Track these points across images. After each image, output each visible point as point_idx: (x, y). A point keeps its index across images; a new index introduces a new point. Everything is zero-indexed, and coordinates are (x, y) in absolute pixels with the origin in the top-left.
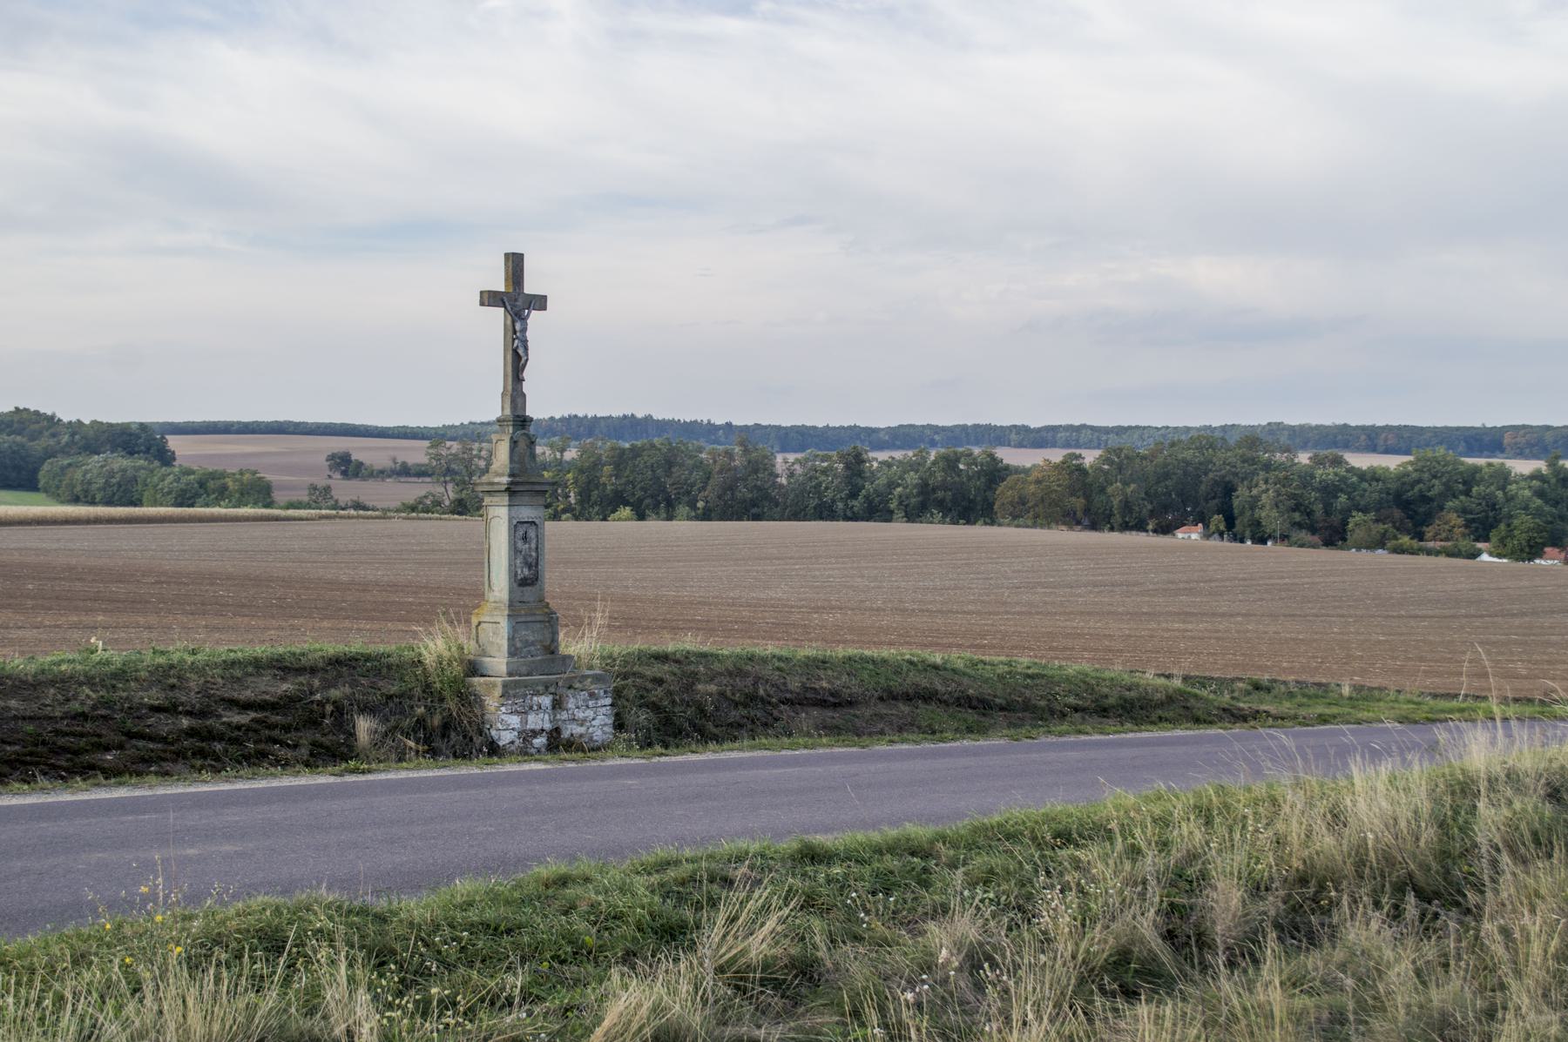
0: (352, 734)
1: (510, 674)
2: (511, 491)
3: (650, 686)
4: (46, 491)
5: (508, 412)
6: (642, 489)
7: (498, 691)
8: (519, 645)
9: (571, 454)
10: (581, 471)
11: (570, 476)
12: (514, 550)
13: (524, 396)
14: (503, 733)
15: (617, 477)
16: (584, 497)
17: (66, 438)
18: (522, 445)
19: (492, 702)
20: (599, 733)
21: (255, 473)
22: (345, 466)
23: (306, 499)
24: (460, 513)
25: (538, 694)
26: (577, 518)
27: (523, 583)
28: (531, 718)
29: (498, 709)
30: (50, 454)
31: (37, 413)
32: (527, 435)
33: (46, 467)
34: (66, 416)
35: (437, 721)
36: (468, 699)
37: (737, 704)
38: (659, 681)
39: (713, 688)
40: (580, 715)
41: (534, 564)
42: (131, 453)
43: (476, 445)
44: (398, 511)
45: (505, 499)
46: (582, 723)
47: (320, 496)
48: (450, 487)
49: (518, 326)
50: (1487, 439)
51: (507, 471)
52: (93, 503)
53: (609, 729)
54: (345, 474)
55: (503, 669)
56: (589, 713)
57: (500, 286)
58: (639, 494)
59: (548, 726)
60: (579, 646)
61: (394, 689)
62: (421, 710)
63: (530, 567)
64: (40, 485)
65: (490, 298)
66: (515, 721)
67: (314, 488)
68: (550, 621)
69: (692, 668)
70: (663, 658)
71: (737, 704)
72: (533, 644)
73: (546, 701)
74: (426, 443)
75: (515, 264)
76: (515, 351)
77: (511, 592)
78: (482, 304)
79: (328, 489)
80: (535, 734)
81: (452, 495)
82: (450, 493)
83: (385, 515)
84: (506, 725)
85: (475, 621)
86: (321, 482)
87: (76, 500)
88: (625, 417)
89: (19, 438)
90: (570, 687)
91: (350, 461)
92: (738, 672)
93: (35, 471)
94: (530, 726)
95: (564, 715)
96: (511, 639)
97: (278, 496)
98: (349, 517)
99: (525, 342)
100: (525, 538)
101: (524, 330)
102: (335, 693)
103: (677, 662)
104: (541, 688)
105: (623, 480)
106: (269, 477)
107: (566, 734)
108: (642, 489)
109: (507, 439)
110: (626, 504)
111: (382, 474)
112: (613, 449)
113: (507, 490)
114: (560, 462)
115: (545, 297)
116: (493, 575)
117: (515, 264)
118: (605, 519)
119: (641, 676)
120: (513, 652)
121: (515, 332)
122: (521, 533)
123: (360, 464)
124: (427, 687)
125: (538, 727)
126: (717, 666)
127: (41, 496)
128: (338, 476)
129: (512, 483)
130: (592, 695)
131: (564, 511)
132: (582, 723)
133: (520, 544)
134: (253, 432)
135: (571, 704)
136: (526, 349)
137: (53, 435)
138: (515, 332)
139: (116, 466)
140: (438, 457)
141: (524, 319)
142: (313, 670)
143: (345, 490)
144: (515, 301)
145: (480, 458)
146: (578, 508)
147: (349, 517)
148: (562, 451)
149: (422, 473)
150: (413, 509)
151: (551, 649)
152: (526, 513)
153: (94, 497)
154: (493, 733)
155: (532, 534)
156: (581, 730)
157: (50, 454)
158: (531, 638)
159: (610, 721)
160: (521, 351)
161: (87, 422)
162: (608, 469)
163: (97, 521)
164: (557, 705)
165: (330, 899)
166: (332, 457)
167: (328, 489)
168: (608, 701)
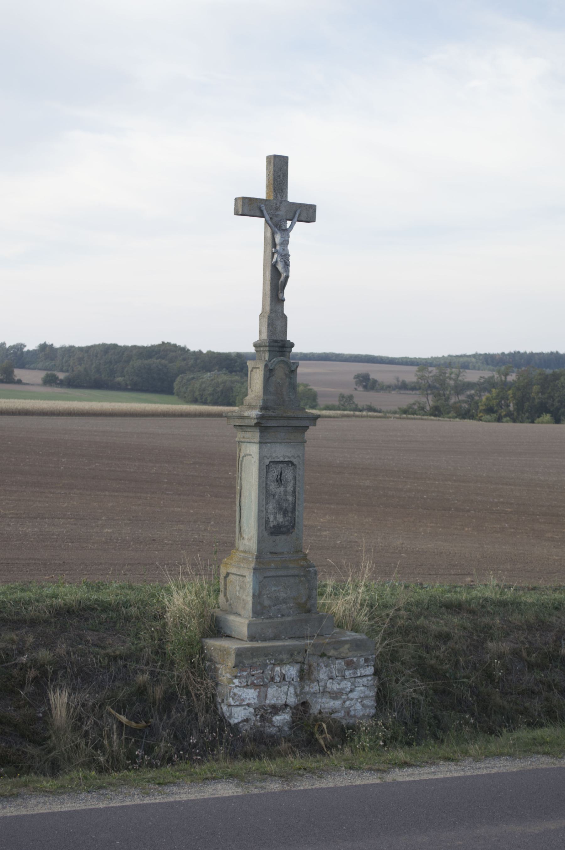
0: (49, 712)
1: (252, 638)
2: (262, 425)
3: (431, 642)
4: (178, 395)
5: (265, 336)
6: (559, 401)
7: (231, 662)
8: (267, 602)
9: (512, 378)
10: (518, 389)
11: (510, 392)
12: (265, 494)
13: (285, 318)
14: (235, 710)
15: (543, 393)
16: (520, 406)
17: (191, 362)
18: (280, 373)
19: (225, 673)
20: (359, 706)
21: (306, 386)
22: (366, 382)
23: (337, 403)
24: (435, 416)
25: (281, 663)
26: (514, 421)
27: (277, 531)
28: (272, 691)
29: (230, 681)
30: (182, 371)
31: (175, 345)
32: (286, 363)
33: (178, 379)
34: (193, 348)
35: (159, 692)
36: (201, 666)
37: (531, 667)
38: (445, 637)
39: (505, 647)
40: (334, 686)
41: (289, 511)
42: (231, 372)
43: (448, 370)
44: (395, 413)
45: (256, 435)
46: (335, 695)
47: (346, 402)
48: (430, 397)
49: (278, 239)
50: (397, 361)
51: (261, 403)
52: (205, 403)
53: (371, 702)
54: (365, 387)
55: (244, 631)
56: (347, 685)
57: (259, 190)
58: (557, 404)
59: (292, 700)
60: (345, 598)
61: (121, 649)
62: (143, 678)
63: (285, 512)
64: (175, 391)
65: (247, 207)
66: (251, 695)
67: (342, 396)
68: (307, 574)
69: (486, 620)
70: (454, 607)
71: (531, 667)
72: (284, 601)
73: (292, 671)
74: (415, 368)
75: (278, 167)
76: (274, 267)
77: (260, 541)
78: (237, 213)
79: (351, 397)
80: (276, 709)
81: (431, 403)
82: (430, 402)
83: (385, 415)
84: (240, 702)
85: (223, 572)
86: (347, 392)
87: (195, 401)
88: (552, 353)
89: (163, 361)
90: (323, 655)
91: (369, 379)
92: (542, 626)
93: (173, 381)
94: (271, 700)
95: (315, 688)
96: (257, 597)
97: (321, 402)
98: (362, 417)
99: (286, 258)
100: (279, 480)
101: (285, 243)
102: (44, 654)
103: (472, 612)
104: (284, 657)
105: (546, 395)
106: (315, 388)
107: (314, 710)
108: (559, 401)
109: (261, 366)
110: (547, 411)
111: (389, 388)
112: (540, 374)
113: (257, 425)
114: (505, 383)
115: (312, 208)
116: (244, 520)
117: (278, 167)
118: (533, 422)
119: (424, 631)
120: (259, 610)
121: (274, 245)
122: (274, 473)
123: (375, 382)
124: (160, 651)
125: (281, 702)
126: (516, 618)
127: (174, 398)
128: (361, 389)
129: (261, 417)
130: (350, 664)
131: (506, 416)
132: (335, 695)
133: (273, 487)
134: (310, 359)
135: (323, 675)
136: (287, 265)
137: (184, 359)
138: (274, 245)
139: (220, 380)
140: (422, 377)
141: (286, 232)
142: (33, 623)
143: (363, 398)
144: (277, 209)
145: (450, 379)
146: (515, 414)
147: (362, 417)
148: (506, 375)
149: (404, 387)
150: (405, 412)
151: (307, 608)
152: (281, 452)
153: (206, 399)
154: (225, 708)
155: (288, 474)
156: (337, 704)
157: (182, 371)
158: (283, 595)
159: (372, 693)
160: (280, 267)
161: (205, 351)
162: (536, 388)
163: (201, 415)
164: (305, 675)
165: (396, 629)
166: (357, 377)
167: (351, 397)
168: (370, 670)
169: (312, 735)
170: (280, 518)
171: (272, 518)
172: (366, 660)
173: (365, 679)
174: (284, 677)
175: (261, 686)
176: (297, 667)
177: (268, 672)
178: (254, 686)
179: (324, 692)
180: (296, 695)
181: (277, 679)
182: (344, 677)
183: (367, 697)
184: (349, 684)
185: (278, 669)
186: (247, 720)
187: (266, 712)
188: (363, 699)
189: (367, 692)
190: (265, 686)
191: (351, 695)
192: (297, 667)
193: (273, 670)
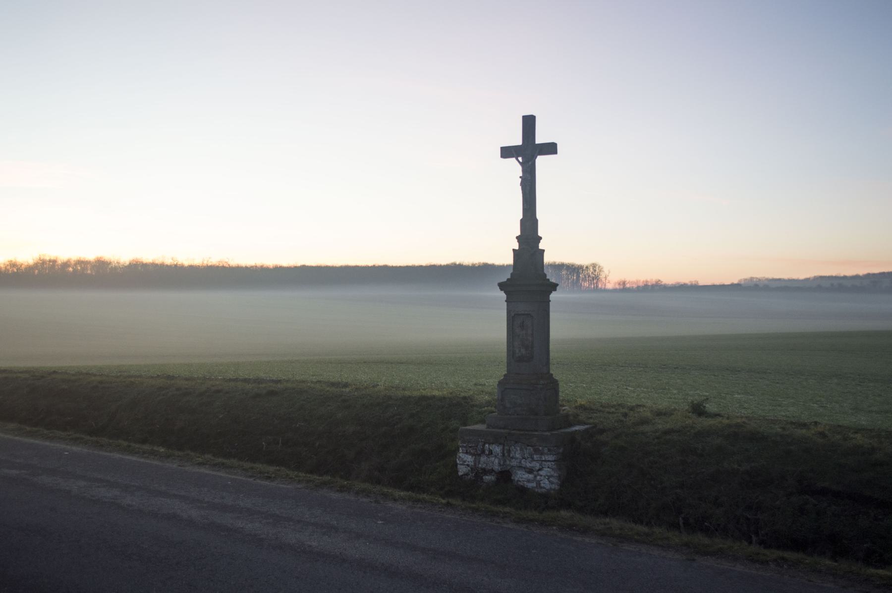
8: (508, 405)
20: (546, 481)
28: (483, 459)
66: (469, 459)
75: (529, 123)
80: (485, 472)
84: (465, 461)
117: (529, 123)
130: (537, 451)
132: (530, 471)
161: (541, 246)
169: (504, 492)
170: (523, 351)
171: (517, 351)
172: (549, 450)
173: (549, 463)
174: (491, 452)
175: (477, 455)
176: (501, 447)
177: (480, 447)
179: (520, 467)
180: (500, 464)
181: (487, 452)
182: (532, 458)
183: (552, 476)
184: (538, 465)
185: (487, 445)
186: (467, 474)
187: (479, 473)
188: (549, 477)
189: (552, 473)
190: (480, 455)
192: (501, 447)
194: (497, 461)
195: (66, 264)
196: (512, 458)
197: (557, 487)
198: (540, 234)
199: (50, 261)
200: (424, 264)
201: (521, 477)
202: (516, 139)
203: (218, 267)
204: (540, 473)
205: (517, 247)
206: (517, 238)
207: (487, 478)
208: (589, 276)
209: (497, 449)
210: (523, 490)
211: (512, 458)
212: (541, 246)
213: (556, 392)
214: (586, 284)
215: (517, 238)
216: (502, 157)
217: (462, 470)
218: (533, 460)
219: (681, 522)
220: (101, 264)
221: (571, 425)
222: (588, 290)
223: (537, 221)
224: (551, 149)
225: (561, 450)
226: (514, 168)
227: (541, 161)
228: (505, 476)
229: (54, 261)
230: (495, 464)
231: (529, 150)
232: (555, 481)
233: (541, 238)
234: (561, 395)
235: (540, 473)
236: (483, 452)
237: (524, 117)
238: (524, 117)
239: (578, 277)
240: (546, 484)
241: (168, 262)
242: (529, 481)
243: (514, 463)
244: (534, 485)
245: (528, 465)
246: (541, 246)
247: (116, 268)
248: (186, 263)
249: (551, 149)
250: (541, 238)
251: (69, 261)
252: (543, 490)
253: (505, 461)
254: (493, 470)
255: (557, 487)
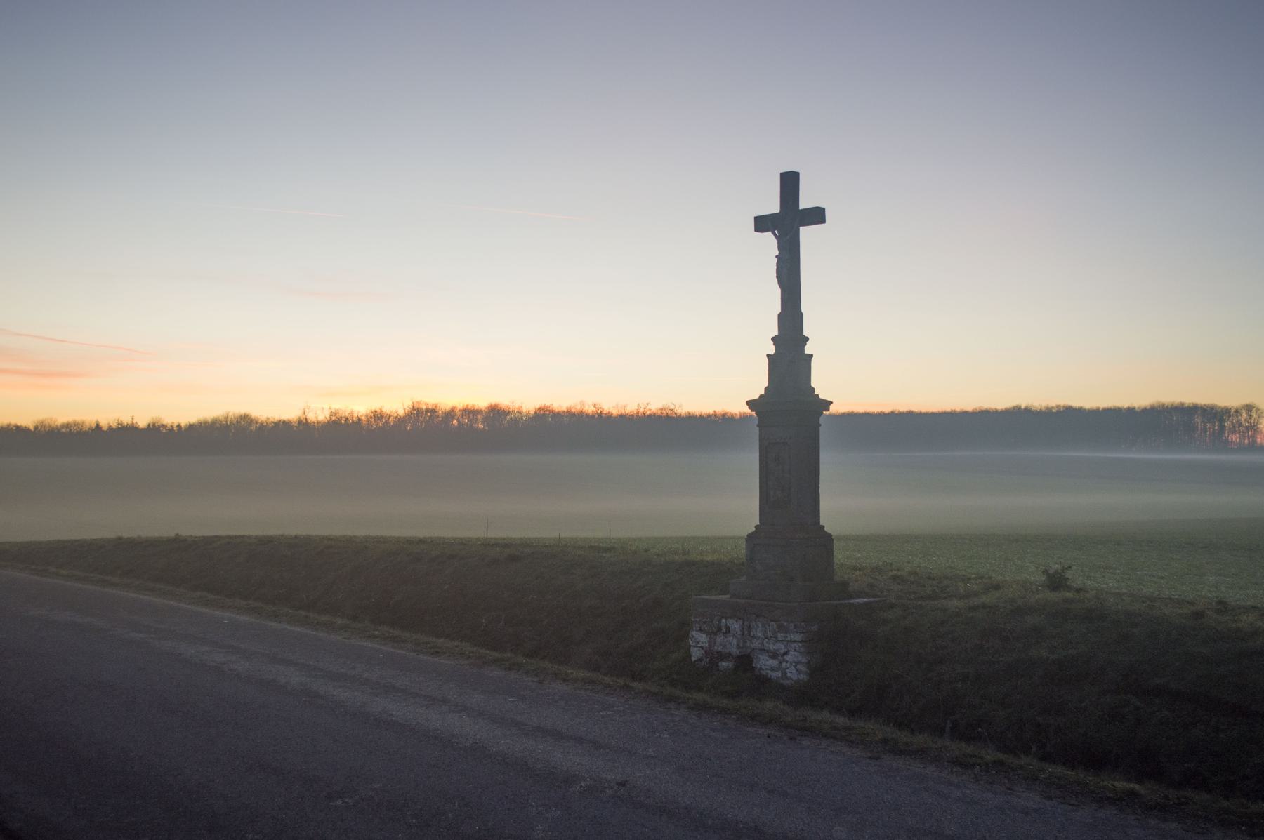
20: (793, 669)
28: (719, 639)
66: (703, 639)
75: (790, 182)
80: (722, 656)
84: (699, 641)
117: (790, 182)
132: (774, 655)
169: (740, 684)
175: (711, 634)
178: (707, 633)
179: (762, 650)
180: (738, 647)
186: (700, 660)
187: (714, 657)
188: (797, 663)
190: (715, 634)
191: (787, 658)
192: (740, 622)
193: (720, 621)
194: (735, 642)
195: (450, 414)
196: (754, 637)
197: (804, 677)
198: (805, 334)
199: (427, 410)
200: (969, 408)
201: (764, 663)
202: (772, 206)
203: (660, 417)
204: (785, 659)
205: (772, 351)
206: (773, 339)
207: (724, 665)
208: (1240, 425)
209: (735, 625)
210: (763, 681)
211: (754, 637)
212: (808, 350)
213: (830, 552)
214: (1235, 438)
215: (773, 339)
216: (757, 230)
217: (696, 654)
218: (777, 641)
219: (949, 725)
220: (496, 413)
221: (851, 597)
222: (1241, 448)
223: (802, 315)
224: (817, 216)
225: (815, 628)
226: (769, 243)
227: (807, 234)
228: (745, 661)
229: (433, 411)
230: (731, 645)
231: (789, 220)
232: (804, 669)
233: (807, 339)
234: (836, 561)
235: (785, 659)
236: (719, 629)
237: (782, 175)
238: (782, 175)
239: (1222, 428)
240: (793, 674)
241: (589, 409)
242: (773, 669)
243: (756, 644)
244: (779, 674)
245: (772, 647)
246: (808, 350)
247: (515, 422)
248: (615, 412)
249: (817, 216)
250: (807, 339)
251: (453, 410)
252: (789, 682)
253: (745, 642)
254: (730, 654)
255: (804, 677)
